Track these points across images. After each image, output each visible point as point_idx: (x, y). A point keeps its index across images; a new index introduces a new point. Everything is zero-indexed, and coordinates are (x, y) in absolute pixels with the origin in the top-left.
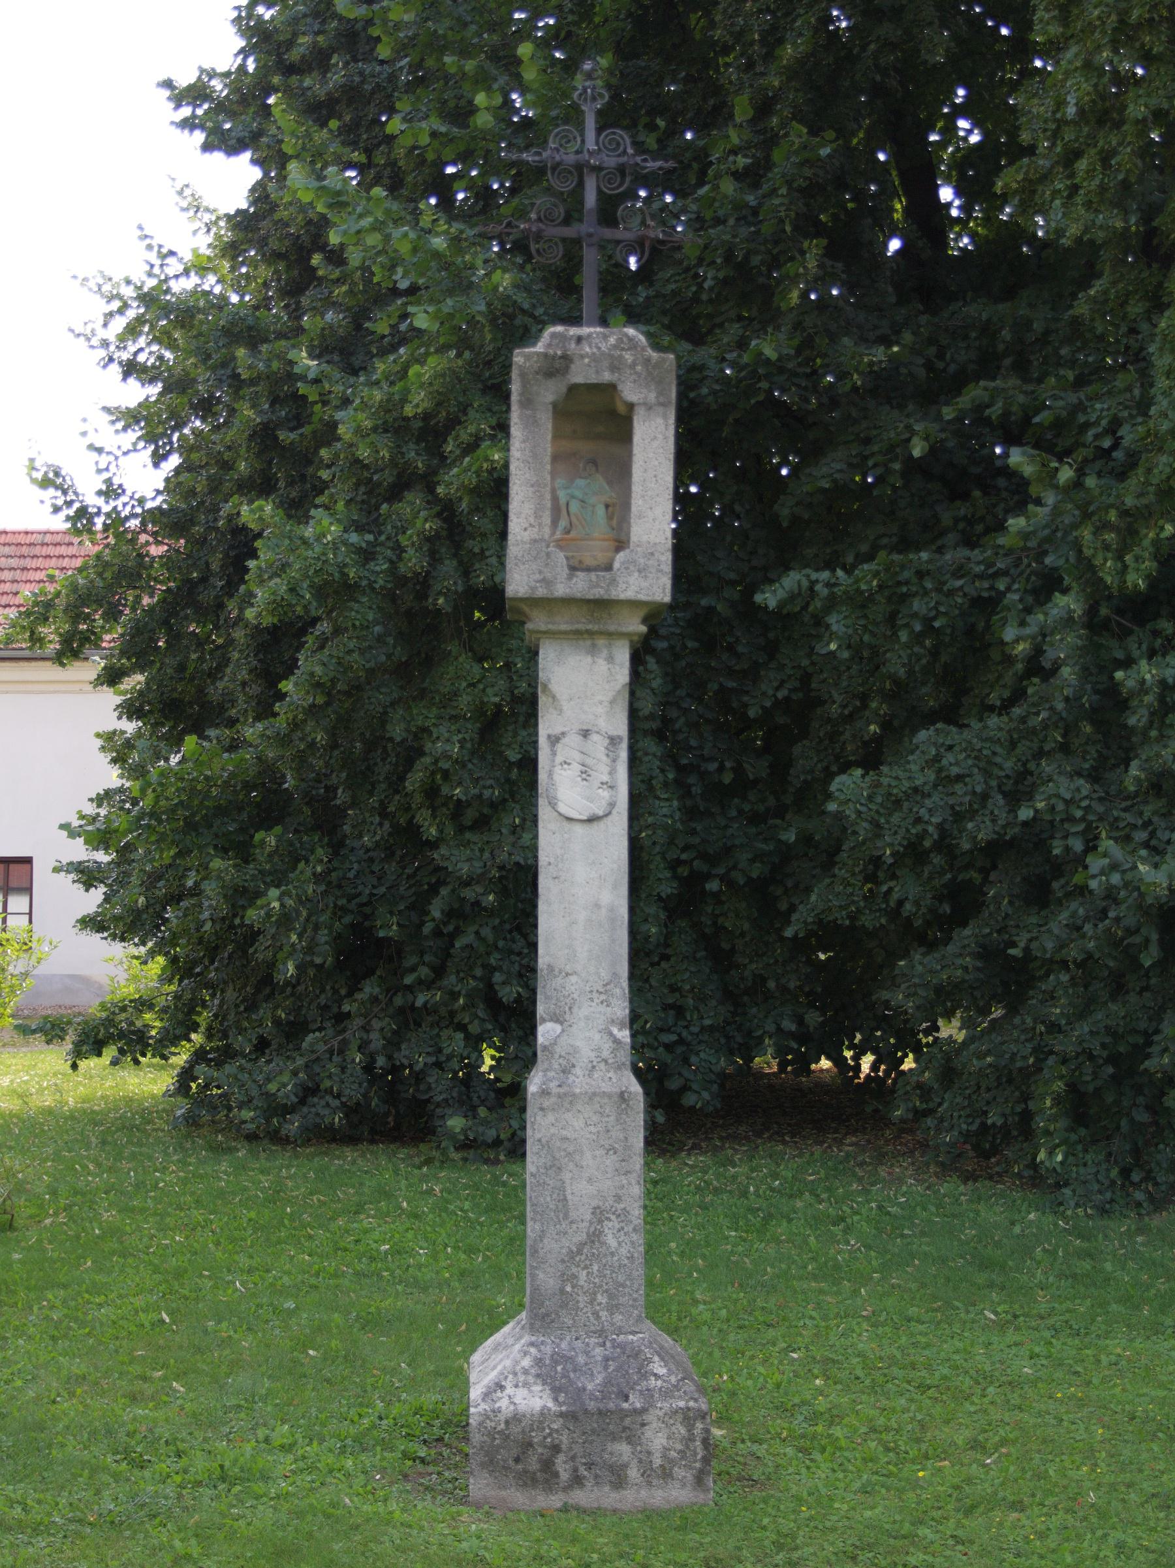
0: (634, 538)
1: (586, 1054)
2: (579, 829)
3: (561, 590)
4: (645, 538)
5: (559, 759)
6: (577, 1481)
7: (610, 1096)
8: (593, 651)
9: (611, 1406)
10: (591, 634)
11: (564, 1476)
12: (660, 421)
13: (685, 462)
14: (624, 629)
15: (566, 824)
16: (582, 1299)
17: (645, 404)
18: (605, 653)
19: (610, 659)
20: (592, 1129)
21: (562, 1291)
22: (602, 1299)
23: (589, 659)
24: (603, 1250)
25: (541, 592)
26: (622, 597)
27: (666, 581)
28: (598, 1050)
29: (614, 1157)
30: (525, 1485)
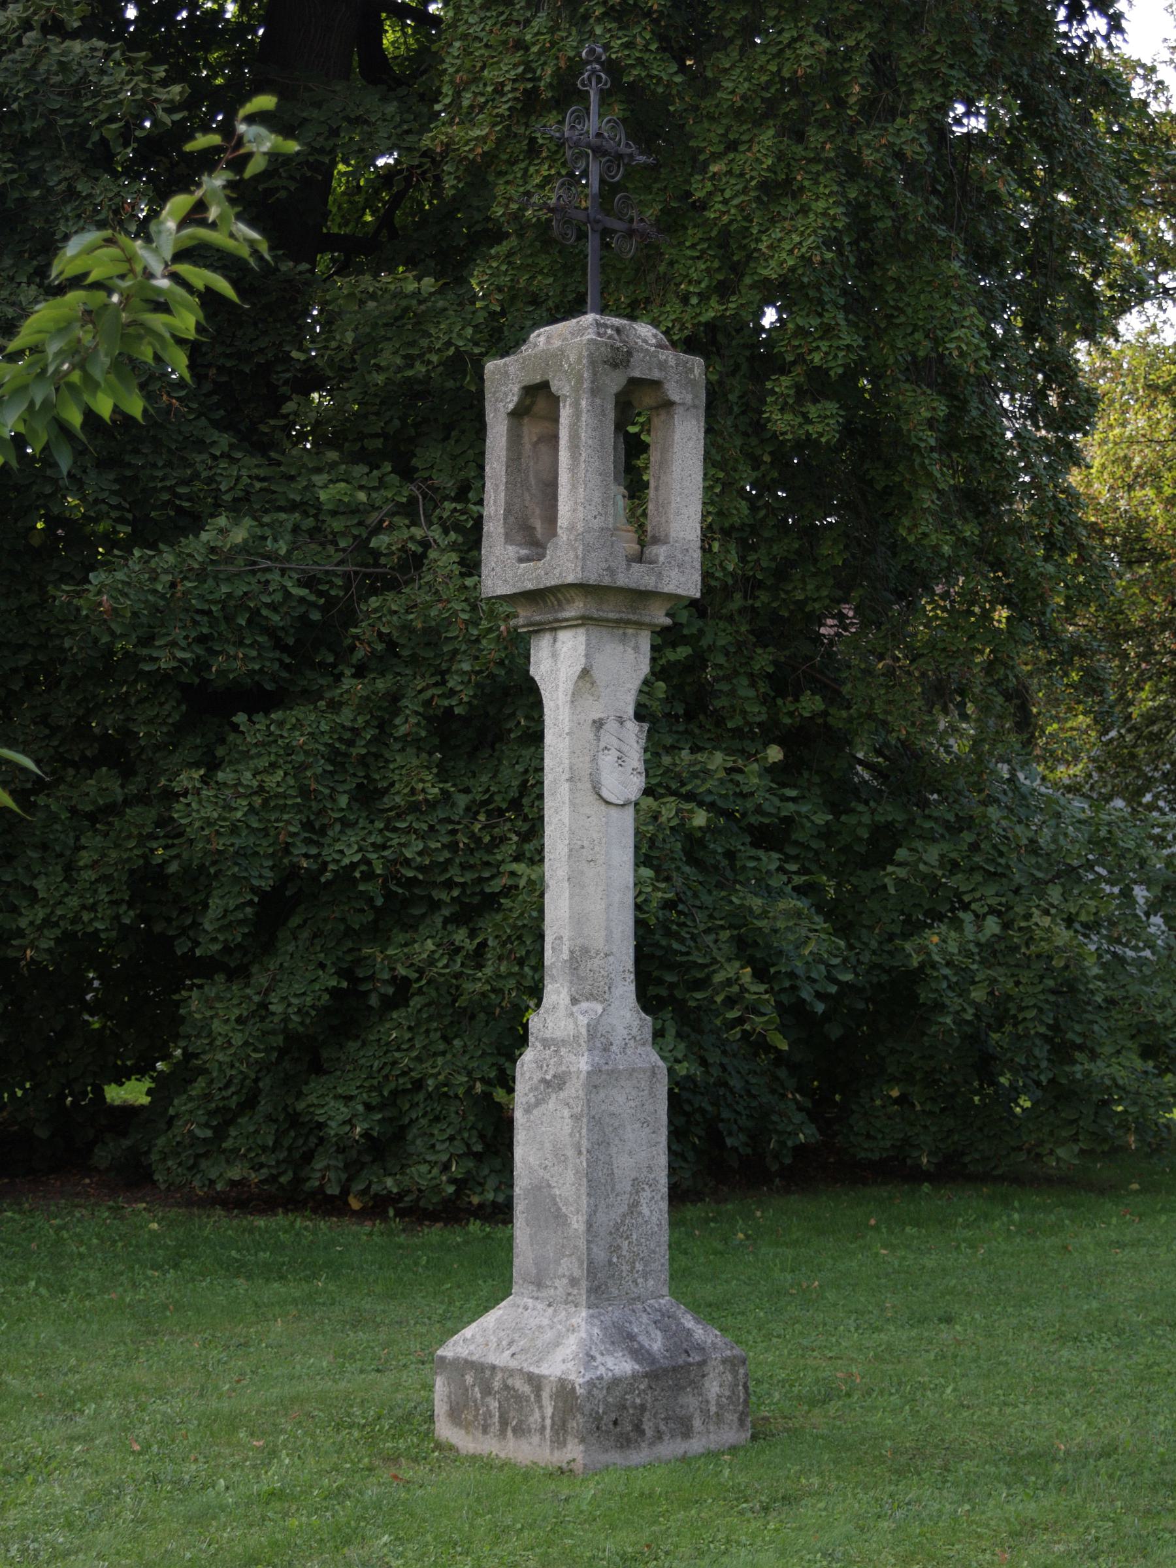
0: (673, 534)
1: (621, 1033)
2: (614, 812)
3: (622, 580)
4: (682, 535)
5: (602, 744)
6: (659, 1436)
7: (644, 1071)
8: (624, 638)
9: (681, 1362)
10: (628, 622)
11: (649, 1433)
12: (694, 422)
13: (716, 460)
14: (647, 619)
15: (603, 807)
16: (625, 1268)
17: (683, 404)
18: (632, 644)
19: (636, 649)
20: (632, 1104)
21: (610, 1262)
22: (639, 1266)
23: (621, 648)
24: (640, 1220)
25: (607, 581)
26: (666, 590)
27: (697, 577)
28: (629, 1027)
29: (647, 1130)
30: (622, 1446)
